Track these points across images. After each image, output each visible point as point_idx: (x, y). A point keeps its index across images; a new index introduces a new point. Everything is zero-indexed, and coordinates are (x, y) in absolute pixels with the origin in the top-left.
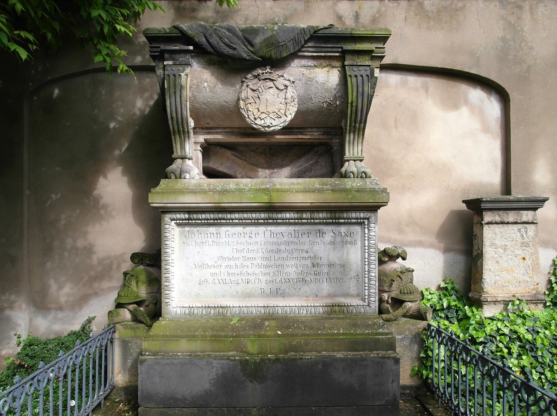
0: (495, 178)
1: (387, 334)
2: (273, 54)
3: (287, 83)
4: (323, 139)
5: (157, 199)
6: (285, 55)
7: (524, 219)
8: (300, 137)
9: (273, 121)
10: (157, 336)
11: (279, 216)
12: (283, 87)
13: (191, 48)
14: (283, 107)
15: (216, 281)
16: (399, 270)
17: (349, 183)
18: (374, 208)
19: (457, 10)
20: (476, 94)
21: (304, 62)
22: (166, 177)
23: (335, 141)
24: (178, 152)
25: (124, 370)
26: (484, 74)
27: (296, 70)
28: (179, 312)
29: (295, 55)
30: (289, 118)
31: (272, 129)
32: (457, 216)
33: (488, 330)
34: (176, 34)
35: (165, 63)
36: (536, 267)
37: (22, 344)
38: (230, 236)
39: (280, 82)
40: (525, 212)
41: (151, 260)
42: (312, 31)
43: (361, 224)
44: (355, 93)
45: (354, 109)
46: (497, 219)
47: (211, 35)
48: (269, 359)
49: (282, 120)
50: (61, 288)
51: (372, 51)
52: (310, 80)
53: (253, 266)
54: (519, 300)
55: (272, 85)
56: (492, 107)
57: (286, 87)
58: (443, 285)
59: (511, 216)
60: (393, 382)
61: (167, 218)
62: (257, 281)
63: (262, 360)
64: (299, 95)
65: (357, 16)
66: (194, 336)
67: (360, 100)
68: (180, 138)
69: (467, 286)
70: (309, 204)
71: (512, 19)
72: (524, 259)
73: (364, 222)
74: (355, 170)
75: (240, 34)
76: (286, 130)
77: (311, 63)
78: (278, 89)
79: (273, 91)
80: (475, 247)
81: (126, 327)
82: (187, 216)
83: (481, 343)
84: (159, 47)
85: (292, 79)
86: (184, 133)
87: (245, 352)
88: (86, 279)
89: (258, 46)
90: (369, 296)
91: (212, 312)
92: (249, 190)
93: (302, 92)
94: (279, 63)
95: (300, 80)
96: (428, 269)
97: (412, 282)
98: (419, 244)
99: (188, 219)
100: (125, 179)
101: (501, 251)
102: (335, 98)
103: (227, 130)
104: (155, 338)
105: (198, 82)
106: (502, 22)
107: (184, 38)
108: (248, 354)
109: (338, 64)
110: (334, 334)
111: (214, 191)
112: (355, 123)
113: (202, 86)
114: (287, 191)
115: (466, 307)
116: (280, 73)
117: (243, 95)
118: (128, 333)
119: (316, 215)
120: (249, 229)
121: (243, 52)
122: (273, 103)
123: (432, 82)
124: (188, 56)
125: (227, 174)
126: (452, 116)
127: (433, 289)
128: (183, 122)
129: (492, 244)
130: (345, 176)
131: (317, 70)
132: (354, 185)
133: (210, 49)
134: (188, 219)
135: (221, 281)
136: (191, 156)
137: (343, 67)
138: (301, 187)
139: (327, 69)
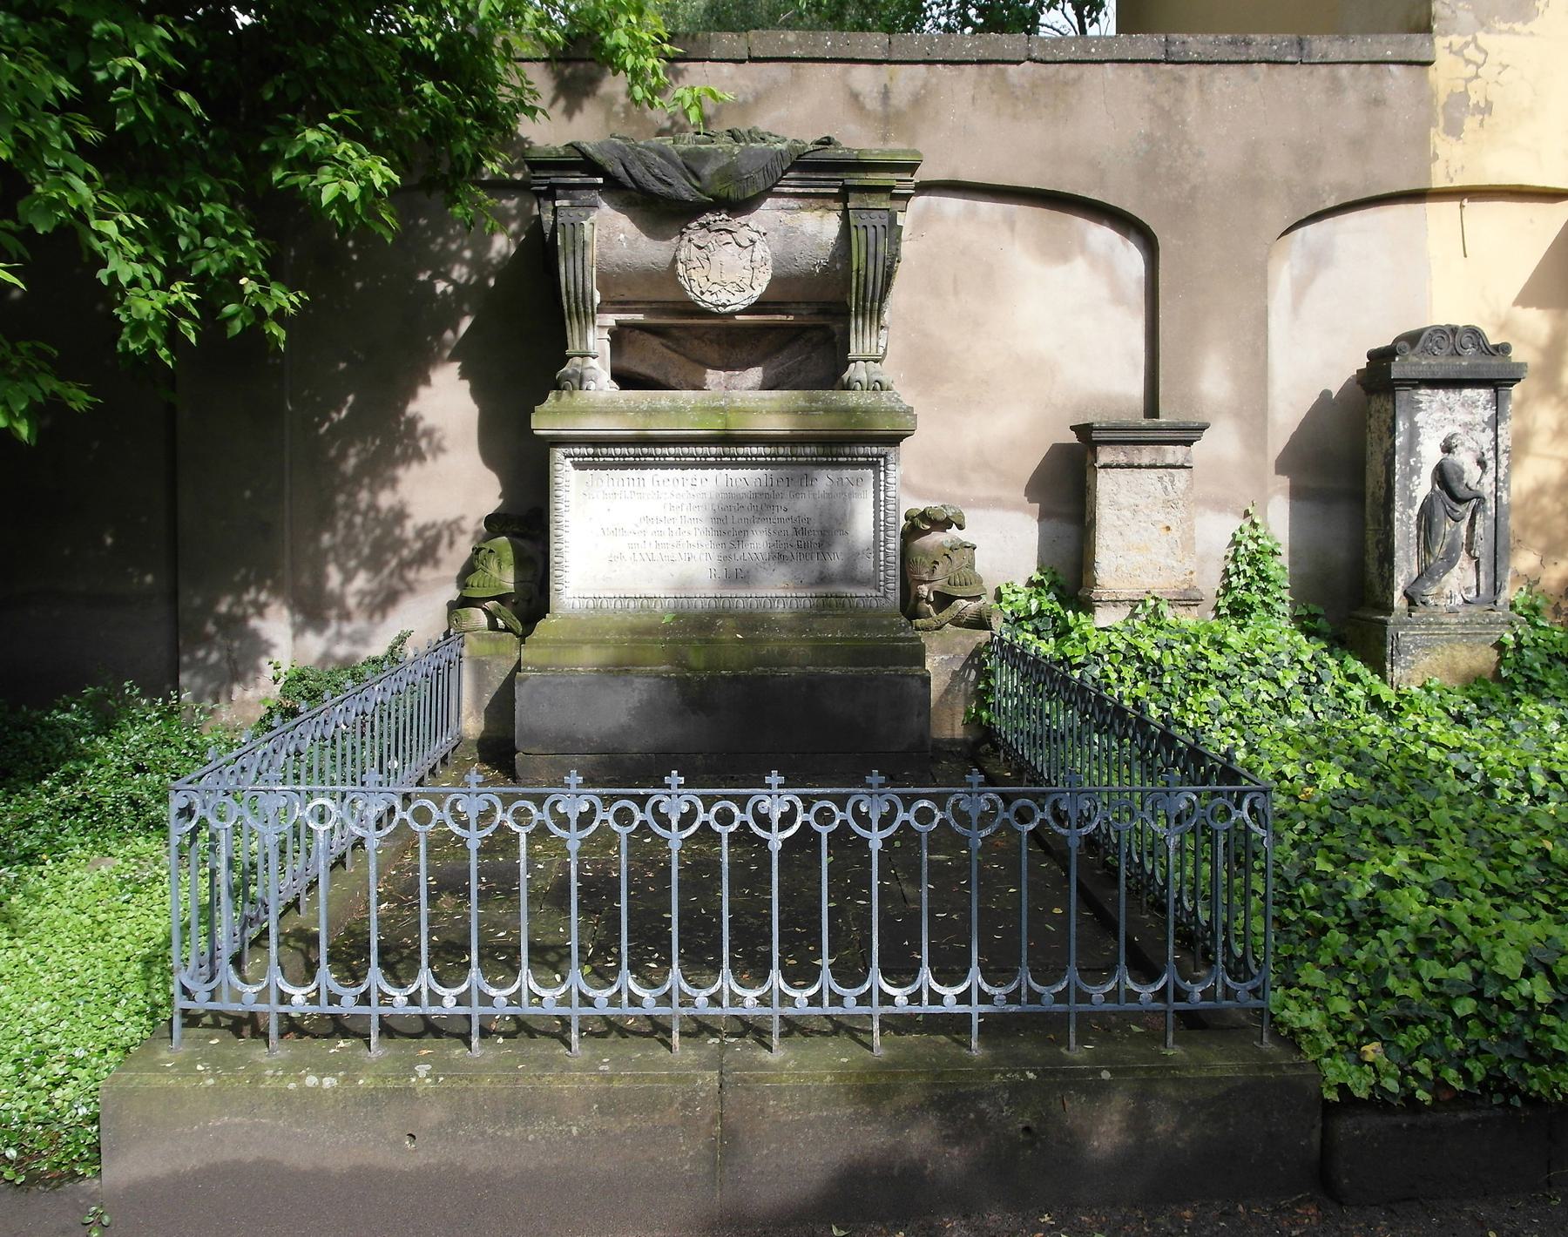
0: (1136, 388)
1: (912, 639)
2: (733, 192)
3: (755, 236)
4: (812, 326)
5: (544, 422)
6: (750, 194)
7: (1170, 460)
8: (779, 317)
9: (730, 297)
10: (544, 641)
11: (741, 450)
13: (600, 180)
15: (638, 557)
16: (948, 545)
17: (852, 398)
18: (894, 440)
19: (1066, 84)
20: (1102, 235)
21: (782, 202)
22: (557, 386)
23: (837, 327)
24: (574, 346)
25: (478, 712)
26: (1111, 201)
27: (768, 213)
28: (577, 605)
29: (768, 193)
30: (758, 292)
32: (1058, 451)
33: (1092, 645)
34: (576, 157)
35: (557, 203)
36: (1188, 543)
37: (282, 680)
39: (744, 235)
41: (526, 523)
42: (795, 156)
43: (874, 465)
44: (863, 255)
45: (862, 279)
46: (1122, 459)
47: (632, 162)
48: (723, 677)
49: (746, 295)
50: (348, 577)
52: (793, 230)
54: (1155, 598)
56: (1132, 259)
57: (753, 242)
58: (1037, 577)
59: (1146, 455)
60: (919, 715)
61: (558, 454)
63: (712, 679)
64: (773, 254)
65: (886, 94)
66: (602, 641)
67: (871, 267)
69: (1070, 577)
71: (1165, 101)
72: (1168, 528)
74: (863, 376)
75: (679, 160)
76: (758, 307)
77: (793, 203)
81: (481, 638)
82: (591, 450)
83: (1078, 666)
85: (763, 230)
86: (585, 315)
87: (684, 666)
88: (394, 563)
89: (707, 180)
90: (886, 580)
91: (632, 604)
92: (693, 409)
93: (778, 248)
94: (740, 206)
95: (776, 230)
96: (1004, 548)
97: (971, 565)
98: (997, 503)
99: (593, 456)
100: (466, 384)
101: (1128, 514)
102: (833, 256)
104: (542, 643)
105: (608, 235)
106: (1147, 106)
107: (588, 164)
108: (690, 669)
109: (838, 205)
110: (827, 639)
111: (637, 411)
112: (865, 300)
113: (615, 239)
114: (745, 411)
115: (1070, 613)
116: (743, 219)
117: (682, 255)
118: (486, 649)
119: (800, 450)
120: (690, 473)
121: (683, 189)
122: (731, 268)
123: (1023, 213)
124: (595, 193)
125: (653, 379)
126: (1058, 272)
127: (1020, 585)
128: (585, 298)
129: (1113, 503)
130: (847, 387)
131: (805, 215)
132: (862, 401)
133: (631, 184)
134: (593, 456)
136: (593, 345)
137: (846, 211)
138: (775, 405)
139: (819, 213)
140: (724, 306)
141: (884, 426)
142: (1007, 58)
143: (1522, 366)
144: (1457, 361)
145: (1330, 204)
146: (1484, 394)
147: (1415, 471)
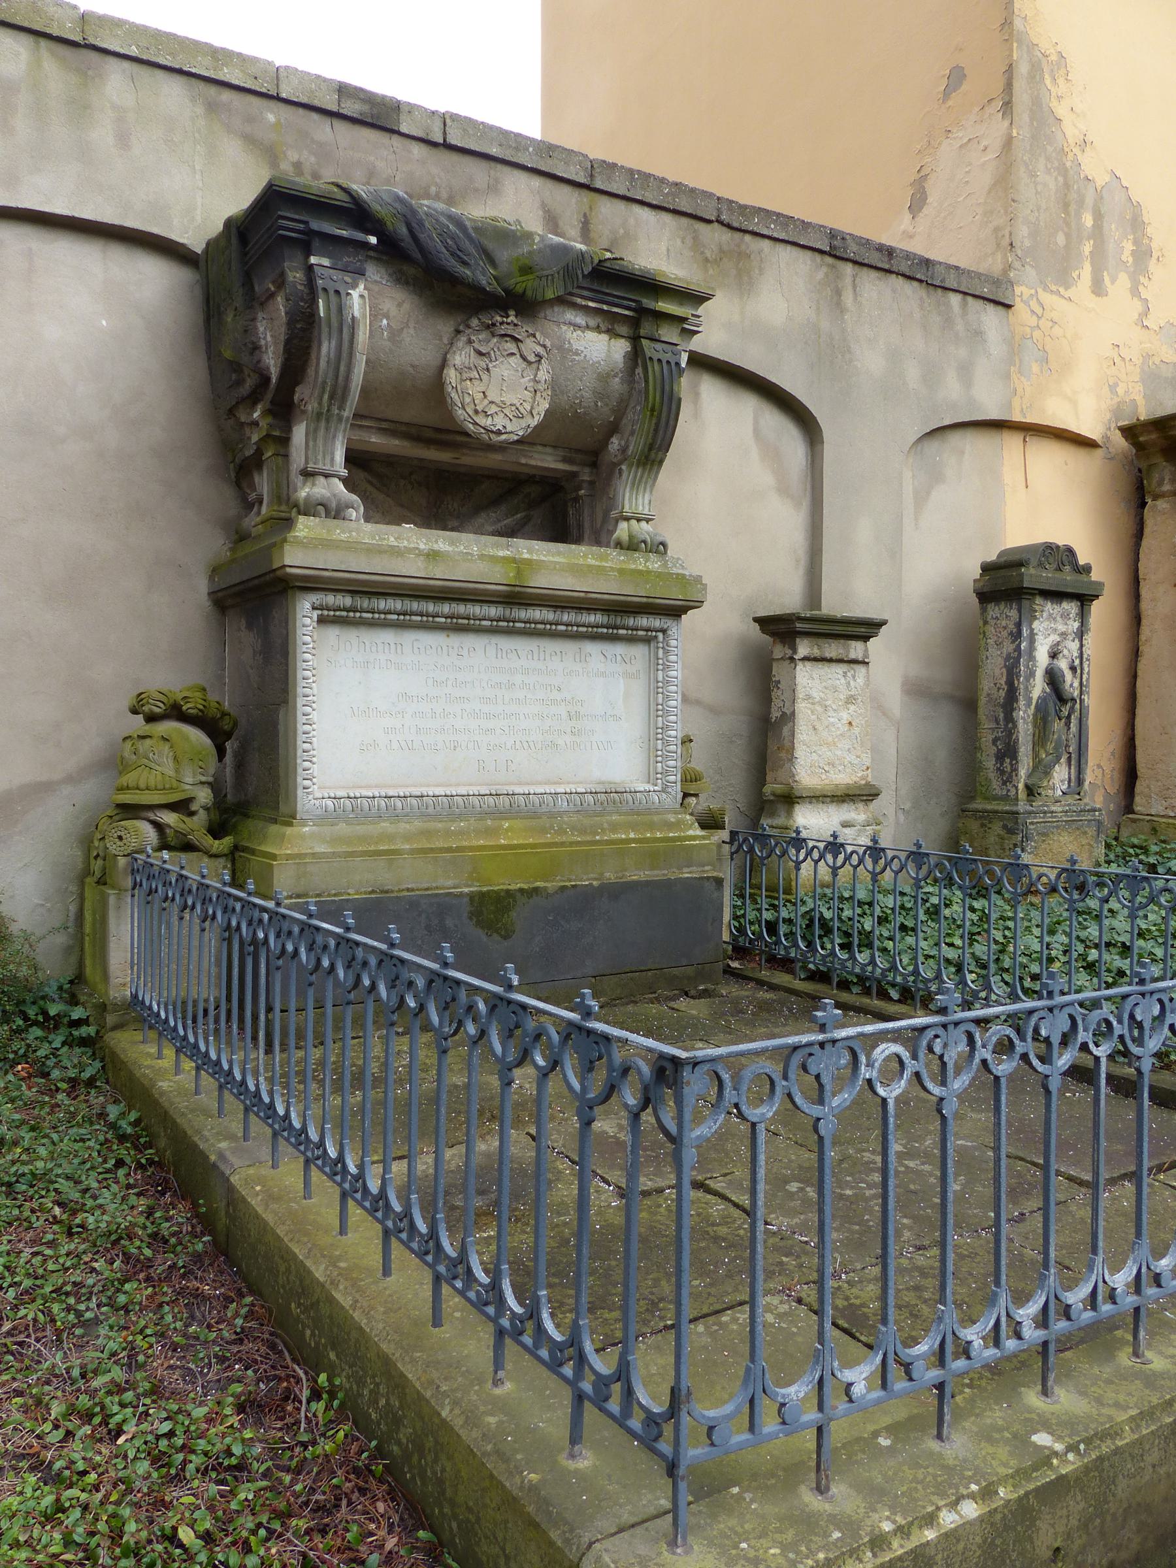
7: (852, 656)
12: (532, 358)
13: (373, 240)
14: (528, 395)
15: (395, 745)
18: (676, 612)
30: (534, 422)
31: (503, 437)
35: (313, 260)
38: (422, 650)
40: (853, 643)
42: (596, 261)
43: (647, 641)
51: (683, 320)
53: (465, 715)
55: (515, 351)
59: (832, 649)
62: (471, 745)
68: (327, 429)
70: (582, 595)
73: (656, 637)
78: (524, 358)
79: (515, 361)
80: (776, 703)
82: (348, 601)
84: (306, 223)
91: (399, 804)
103: (384, 425)
109: (624, 330)
129: (808, 697)
131: (590, 335)
133: (417, 255)
135: (403, 744)
140: (499, 433)
141: (674, 594)
142: (700, 214)
143: (1100, 585)
144: (1058, 575)
145: (947, 422)
146: (1071, 607)
147: (1032, 674)
